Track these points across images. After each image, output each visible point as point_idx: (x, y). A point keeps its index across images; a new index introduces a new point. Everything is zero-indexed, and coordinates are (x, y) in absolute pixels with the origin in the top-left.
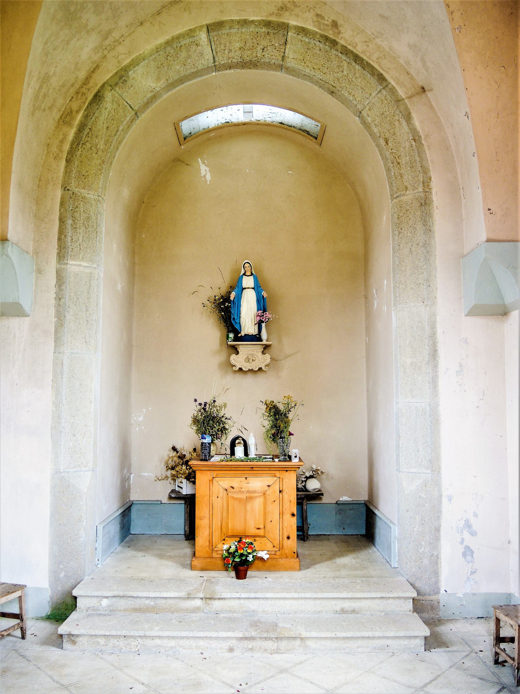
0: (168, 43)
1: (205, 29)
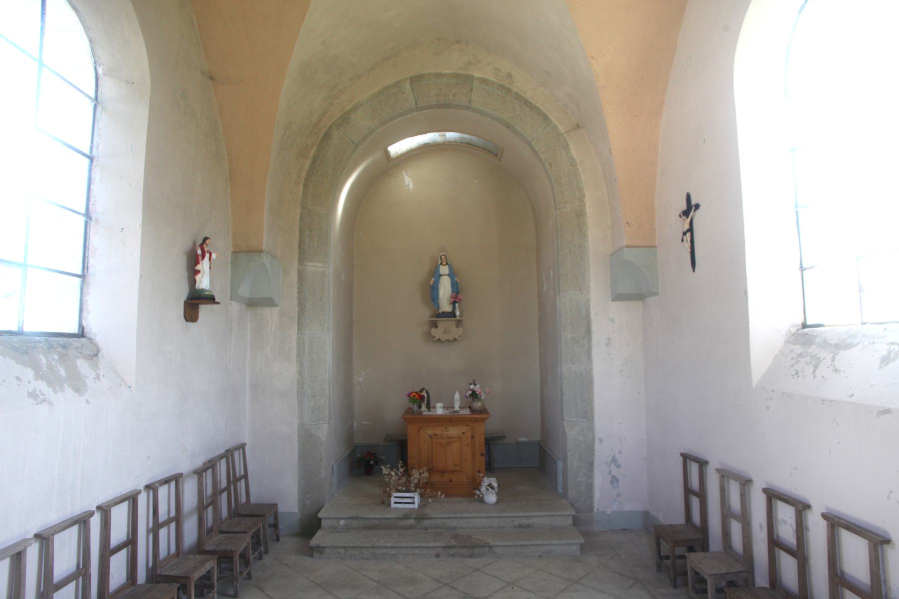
0: (381, 92)
1: (409, 81)
